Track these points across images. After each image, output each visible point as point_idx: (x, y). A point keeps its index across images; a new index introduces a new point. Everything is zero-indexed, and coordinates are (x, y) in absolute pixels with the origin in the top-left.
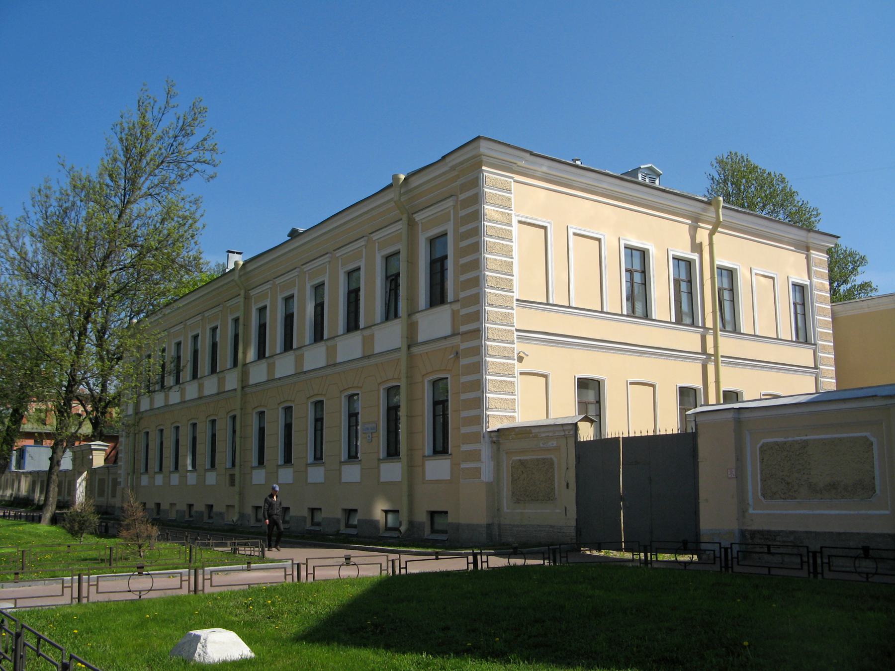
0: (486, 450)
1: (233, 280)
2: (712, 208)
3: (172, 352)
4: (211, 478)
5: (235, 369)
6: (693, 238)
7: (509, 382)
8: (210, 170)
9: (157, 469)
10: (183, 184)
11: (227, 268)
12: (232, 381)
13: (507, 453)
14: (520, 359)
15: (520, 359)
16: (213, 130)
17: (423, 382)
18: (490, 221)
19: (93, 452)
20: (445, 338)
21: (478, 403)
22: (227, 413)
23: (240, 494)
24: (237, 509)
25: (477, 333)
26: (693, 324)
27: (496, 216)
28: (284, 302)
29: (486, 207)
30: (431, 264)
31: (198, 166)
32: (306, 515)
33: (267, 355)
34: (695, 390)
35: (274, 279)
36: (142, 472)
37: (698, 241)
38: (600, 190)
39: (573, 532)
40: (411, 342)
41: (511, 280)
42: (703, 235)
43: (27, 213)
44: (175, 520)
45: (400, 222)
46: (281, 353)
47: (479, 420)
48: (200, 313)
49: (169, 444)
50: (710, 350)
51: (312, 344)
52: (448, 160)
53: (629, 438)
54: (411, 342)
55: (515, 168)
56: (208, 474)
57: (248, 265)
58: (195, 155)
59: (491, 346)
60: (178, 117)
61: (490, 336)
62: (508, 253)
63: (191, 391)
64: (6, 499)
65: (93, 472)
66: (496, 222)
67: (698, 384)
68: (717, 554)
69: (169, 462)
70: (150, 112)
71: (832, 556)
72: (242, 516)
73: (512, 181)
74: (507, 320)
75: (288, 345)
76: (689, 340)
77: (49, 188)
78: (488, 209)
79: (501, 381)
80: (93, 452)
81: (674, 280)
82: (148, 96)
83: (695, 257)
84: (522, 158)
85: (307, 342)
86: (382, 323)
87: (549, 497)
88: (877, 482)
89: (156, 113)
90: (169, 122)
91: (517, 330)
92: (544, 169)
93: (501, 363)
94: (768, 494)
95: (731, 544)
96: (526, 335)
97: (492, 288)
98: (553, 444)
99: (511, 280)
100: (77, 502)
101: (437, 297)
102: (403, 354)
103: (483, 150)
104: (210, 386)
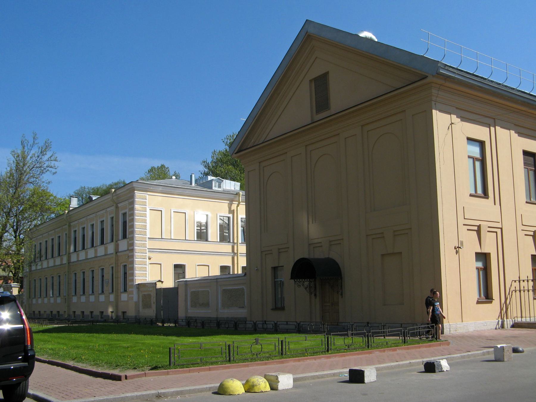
0: (135, 291)
3: (38, 249)
4: (59, 300)
5: (113, 243)
6: (230, 208)
7: (144, 267)
8: (54, 170)
10: (43, 175)
12: (111, 248)
13: (141, 292)
14: (150, 259)
16: (55, 152)
17: (121, 265)
18: (137, 211)
19: (13, 288)
20: (125, 251)
21: (133, 275)
23: (68, 306)
24: (67, 312)
25: (132, 250)
26: (229, 242)
27: (140, 209)
28: (82, 230)
29: (136, 206)
30: (123, 223)
32: (89, 314)
33: (105, 243)
34: (229, 267)
35: (96, 212)
37: (232, 209)
39: (155, 317)
40: (117, 252)
42: (234, 207)
45: (113, 207)
46: (90, 248)
47: (133, 280)
49: (43, 285)
50: (236, 251)
51: (122, 240)
53: (164, 288)
54: (117, 252)
55: (148, 190)
58: (47, 164)
59: (137, 255)
60: (39, 147)
62: (145, 221)
67: (230, 264)
69: (43, 294)
72: (69, 315)
73: (147, 195)
74: (144, 245)
75: (102, 243)
76: (227, 248)
78: (137, 206)
79: (141, 267)
80: (13, 288)
81: (220, 225)
82: (25, 139)
84: (151, 187)
86: (110, 243)
87: (150, 307)
89: (29, 147)
91: (148, 249)
92: (160, 189)
96: (151, 250)
98: (151, 289)
99: (146, 231)
101: (125, 237)
103: (134, 186)
104: (58, 261)
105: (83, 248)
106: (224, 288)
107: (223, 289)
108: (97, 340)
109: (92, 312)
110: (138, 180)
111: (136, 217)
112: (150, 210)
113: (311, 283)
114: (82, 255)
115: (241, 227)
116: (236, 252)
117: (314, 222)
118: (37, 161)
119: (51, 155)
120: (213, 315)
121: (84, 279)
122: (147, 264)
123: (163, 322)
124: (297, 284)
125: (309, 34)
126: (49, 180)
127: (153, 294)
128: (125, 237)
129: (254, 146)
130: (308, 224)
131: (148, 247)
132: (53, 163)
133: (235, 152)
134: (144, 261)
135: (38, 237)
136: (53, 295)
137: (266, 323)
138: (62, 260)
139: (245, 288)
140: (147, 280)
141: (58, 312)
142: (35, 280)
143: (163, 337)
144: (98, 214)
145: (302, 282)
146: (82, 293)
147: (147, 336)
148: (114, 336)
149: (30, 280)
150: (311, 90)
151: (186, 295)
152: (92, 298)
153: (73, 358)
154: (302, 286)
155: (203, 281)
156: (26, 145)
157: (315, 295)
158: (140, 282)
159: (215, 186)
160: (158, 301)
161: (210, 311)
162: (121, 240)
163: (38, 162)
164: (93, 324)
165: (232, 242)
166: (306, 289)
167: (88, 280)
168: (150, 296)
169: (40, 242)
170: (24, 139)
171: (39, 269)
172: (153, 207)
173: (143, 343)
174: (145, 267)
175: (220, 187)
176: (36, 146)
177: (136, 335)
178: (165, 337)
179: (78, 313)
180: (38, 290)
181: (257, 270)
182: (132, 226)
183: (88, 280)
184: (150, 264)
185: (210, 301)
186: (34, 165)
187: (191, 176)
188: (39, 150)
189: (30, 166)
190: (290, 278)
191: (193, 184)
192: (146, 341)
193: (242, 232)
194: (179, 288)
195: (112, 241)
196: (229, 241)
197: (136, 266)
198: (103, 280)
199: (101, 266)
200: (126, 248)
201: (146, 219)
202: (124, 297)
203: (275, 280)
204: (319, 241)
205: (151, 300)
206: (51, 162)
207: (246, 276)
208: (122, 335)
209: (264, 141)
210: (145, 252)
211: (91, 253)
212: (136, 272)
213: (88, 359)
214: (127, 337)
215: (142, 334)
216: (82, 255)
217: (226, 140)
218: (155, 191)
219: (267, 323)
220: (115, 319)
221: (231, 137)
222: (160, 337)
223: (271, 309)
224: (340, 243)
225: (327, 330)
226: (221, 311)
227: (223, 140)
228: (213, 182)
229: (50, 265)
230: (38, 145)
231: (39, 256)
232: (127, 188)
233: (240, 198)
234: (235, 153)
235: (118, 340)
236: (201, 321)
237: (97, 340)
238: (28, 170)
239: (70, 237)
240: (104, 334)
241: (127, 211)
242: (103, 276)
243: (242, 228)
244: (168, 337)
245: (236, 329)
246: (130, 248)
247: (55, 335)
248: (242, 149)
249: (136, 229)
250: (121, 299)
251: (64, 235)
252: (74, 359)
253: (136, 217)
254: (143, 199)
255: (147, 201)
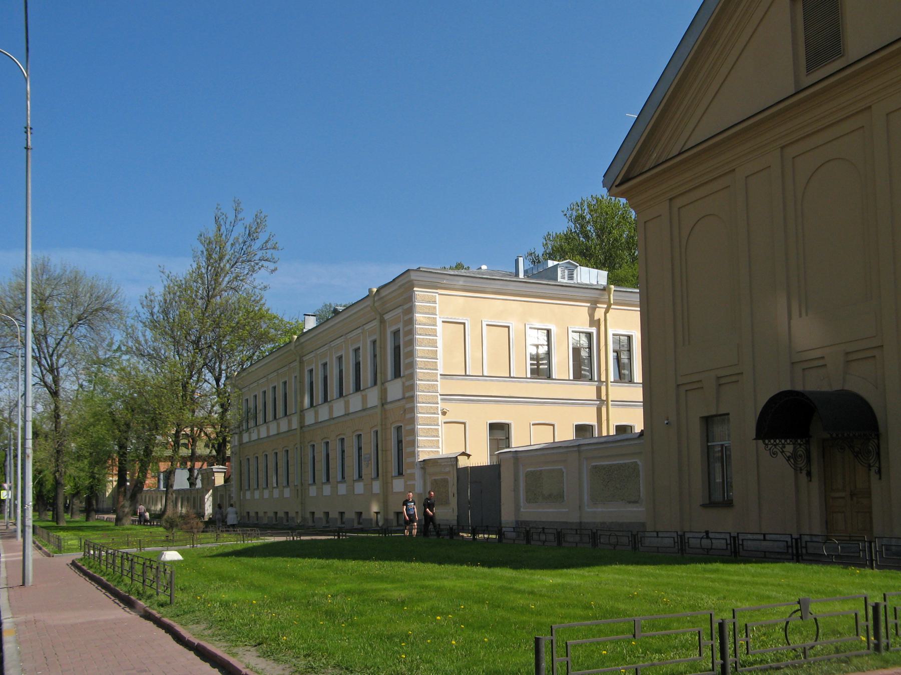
0: (418, 473)
1: (291, 350)
2: (606, 293)
3: (251, 404)
4: (287, 493)
5: (376, 387)
6: (591, 315)
7: (434, 429)
8: (272, 266)
9: (324, 480)
10: (254, 275)
11: (304, 328)
12: (373, 397)
14: (444, 413)
15: (444, 413)
16: (273, 234)
18: (420, 324)
20: (399, 400)
21: (413, 443)
22: (283, 448)
23: (302, 503)
25: (412, 399)
26: (591, 380)
27: (424, 321)
28: (323, 368)
29: (417, 315)
31: (265, 264)
32: (283, 516)
33: (361, 389)
36: (310, 483)
37: (596, 318)
38: (509, 292)
39: (455, 523)
40: (384, 402)
41: (436, 362)
42: (599, 313)
43: (139, 313)
44: (267, 524)
47: (413, 454)
48: (275, 371)
49: (262, 467)
50: (604, 397)
52: (397, 281)
54: (384, 402)
55: (439, 285)
56: (340, 485)
57: (301, 338)
58: (260, 254)
59: (421, 406)
61: (420, 400)
62: (434, 344)
63: (355, 402)
64: (157, 513)
65: (216, 489)
66: (425, 325)
67: (594, 422)
68: (790, 544)
70: (223, 226)
71: (745, 539)
72: (304, 519)
73: (437, 295)
75: (358, 388)
76: (587, 390)
77: (153, 294)
78: (418, 316)
79: (428, 429)
81: (573, 348)
83: (594, 330)
84: (444, 279)
85: (335, 398)
86: (372, 387)
88: (565, 494)
89: (228, 226)
90: (239, 231)
91: (440, 395)
92: (461, 283)
93: (428, 417)
94: (528, 500)
95: (637, 532)
96: (447, 398)
97: (421, 369)
98: (447, 469)
99: (436, 362)
100: (206, 513)
101: (397, 374)
102: (379, 410)
104: (284, 427)
105: (326, 400)
106: (593, 464)
107: (593, 466)
108: (336, 576)
109: (342, 514)
110: (419, 268)
111: (417, 337)
112: (443, 322)
113: (800, 447)
114: (324, 414)
115: (614, 352)
116: (605, 399)
117: (804, 314)
118: (243, 251)
119: (267, 239)
120: (574, 518)
121: (328, 455)
122: (440, 424)
123: (474, 532)
124: (770, 449)
125: (438, 477)
126: (265, 284)
127: (452, 479)
128: (397, 374)
129: (659, 165)
130: (790, 317)
131: (440, 391)
132: (269, 254)
133: (617, 183)
134: (433, 417)
135: (251, 386)
136: (277, 485)
137: (708, 537)
138: (290, 422)
139: (639, 463)
140: (441, 454)
141: (287, 513)
142: (248, 459)
143: (481, 568)
144: (349, 336)
145: (781, 446)
146: (324, 480)
147: (446, 566)
148: (374, 566)
149: (241, 459)
150: (793, 20)
151: (516, 480)
152: (342, 489)
153: (258, 641)
154: (779, 454)
155: (549, 452)
156: (222, 223)
157: (809, 474)
158: (426, 457)
159: (563, 278)
160: (460, 492)
161: (567, 510)
162: (392, 380)
163: (245, 252)
164: (339, 537)
165: (596, 379)
166: (788, 460)
167: (335, 455)
168: (445, 481)
169: (254, 394)
170: (219, 214)
171: (254, 441)
172: (450, 317)
173: (439, 589)
174: (436, 429)
175: (571, 277)
176: (240, 223)
177: (422, 564)
178: (486, 570)
179: (319, 514)
180: (253, 476)
181: (667, 424)
182: (411, 354)
183: (335, 455)
184: (445, 423)
185: (565, 490)
186: (238, 259)
187: (517, 261)
188: (245, 231)
189: (231, 260)
190: (755, 437)
191: (521, 275)
192: (446, 583)
193: (616, 360)
194: (502, 464)
195: (375, 383)
196: (590, 378)
197: (419, 427)
198: (360, 456)
199: (357, 430)
200: (400, 396)
201: (436, 340)
202: (398, 485)
203: (709, 444)
204: (818, 354)
205: (448, 491)
206: (267, 251)
207: (643, 437)
208: (393, 563)
209: (682, 149)
210: (435, 401)
211: (339, 408)
212: (419, 438)
213: (294, 647)
214: (402, 570)
215: (433, 562)
216: (324, 414)
217: (571, 212)
218: (452, 286)
219: (711, 535)
220: (383, 525)
221: (578, 206)
222: (475, 569)
223: (701, 505)
224: (874, 357)
225: (881, 556)
226: (589, 510)
227: (565, 213)
228: (559, 270)
229: (271, 434)
230: (243, 222)
231: (250, 417)
232: (399, 284)
233: (612, 296)
234: (617, 186)
235: (381, 579)
236: (555, 531)
237: (336, 576)
238: (228, 266)
239: (302, 382)
240: (354, 559)
241: (401, 326)
242: (360, 449)
243: (615, 354)
244: (492, 569)
245: (635, 548)
246: (407, 395)
247: (256, 561)
248: (631, 176)
249: (418, 359)
250: (392, 487)
251: (293, 378)
252: (259, 644)
253: (417, 337)
254: (428, 302)
255: (437, 305)
